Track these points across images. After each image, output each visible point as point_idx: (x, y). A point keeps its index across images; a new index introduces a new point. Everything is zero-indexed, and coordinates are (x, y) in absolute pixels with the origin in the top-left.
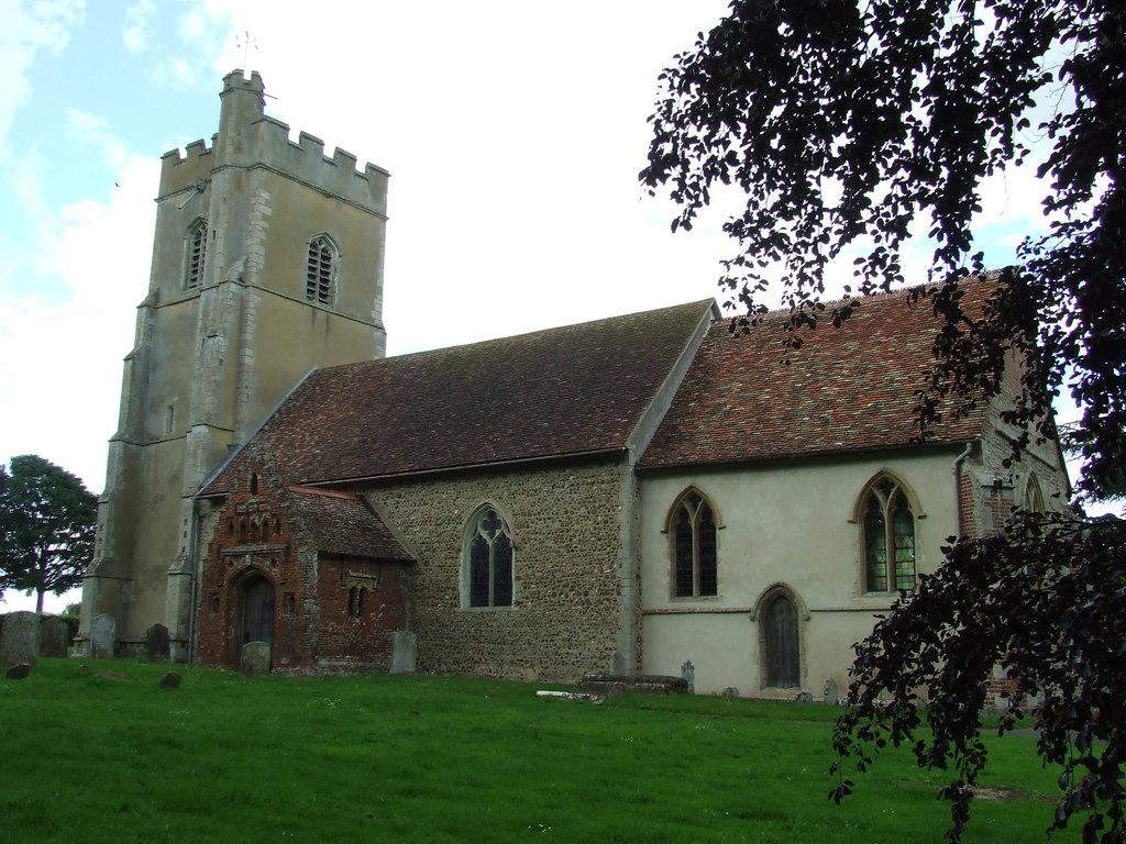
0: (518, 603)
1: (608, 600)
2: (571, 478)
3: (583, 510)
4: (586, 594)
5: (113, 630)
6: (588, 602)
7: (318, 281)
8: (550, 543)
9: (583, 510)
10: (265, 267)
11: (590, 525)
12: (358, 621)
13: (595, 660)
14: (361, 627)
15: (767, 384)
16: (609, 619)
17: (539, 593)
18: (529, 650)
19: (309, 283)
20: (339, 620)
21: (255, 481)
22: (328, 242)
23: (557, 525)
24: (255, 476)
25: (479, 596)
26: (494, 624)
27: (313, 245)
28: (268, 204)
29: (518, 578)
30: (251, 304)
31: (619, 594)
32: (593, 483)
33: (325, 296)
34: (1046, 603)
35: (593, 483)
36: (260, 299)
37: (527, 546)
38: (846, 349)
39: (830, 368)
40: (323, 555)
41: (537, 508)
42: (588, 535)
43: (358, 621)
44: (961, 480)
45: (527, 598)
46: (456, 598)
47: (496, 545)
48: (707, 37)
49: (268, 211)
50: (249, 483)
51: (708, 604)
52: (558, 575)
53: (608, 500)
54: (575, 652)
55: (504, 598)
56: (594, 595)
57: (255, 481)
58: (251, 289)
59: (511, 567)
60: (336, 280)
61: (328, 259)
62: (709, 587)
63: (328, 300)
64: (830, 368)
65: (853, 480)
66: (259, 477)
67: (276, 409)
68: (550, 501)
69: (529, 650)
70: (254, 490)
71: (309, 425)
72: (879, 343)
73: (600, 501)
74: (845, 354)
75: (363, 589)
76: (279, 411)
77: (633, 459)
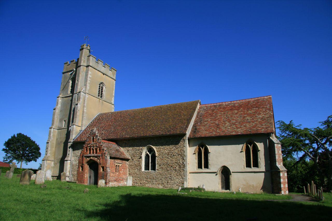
0: (157, 170)
2: (172, 140)
5: (51, 173)
7: (100, 93)
10: (89, 89)
12: (117, 173)
14: (118, 175)
15: (217, 120)
19: (99, 93)
20: (113, 173)
21: (93, 139)
22: (103, 84)
24: (93, 137)
25: (147, 168)
26: (151, 175)
27: (100, 85)
28: (90, 75)
29: (157, 164)
30: (86, 97)
32: (177, 141)
33: (102, 97)
35: (177, 141)
36: (88, 96)
38: (234, 112)
39: (232, 116)
40: (111, 158)
43: (117, 173)
45: (160, 168)
46: (141, 168)
49: (91, 76)
51: (207, 170)
55: (154, 168)
57: (93, 139)
58: (86, 94)
59: (155, 161)
60: (104, 93)
61: (103, 88)
62: (206, 166)
63: (102, 98)
64: (232, 116)
66: (94, 137)
67: (90, 122)
71: (100, 126)
72: (242, 111)
74: (235, 113)
75: (119, 166)
76: (91, 122)
77: (188, 136)
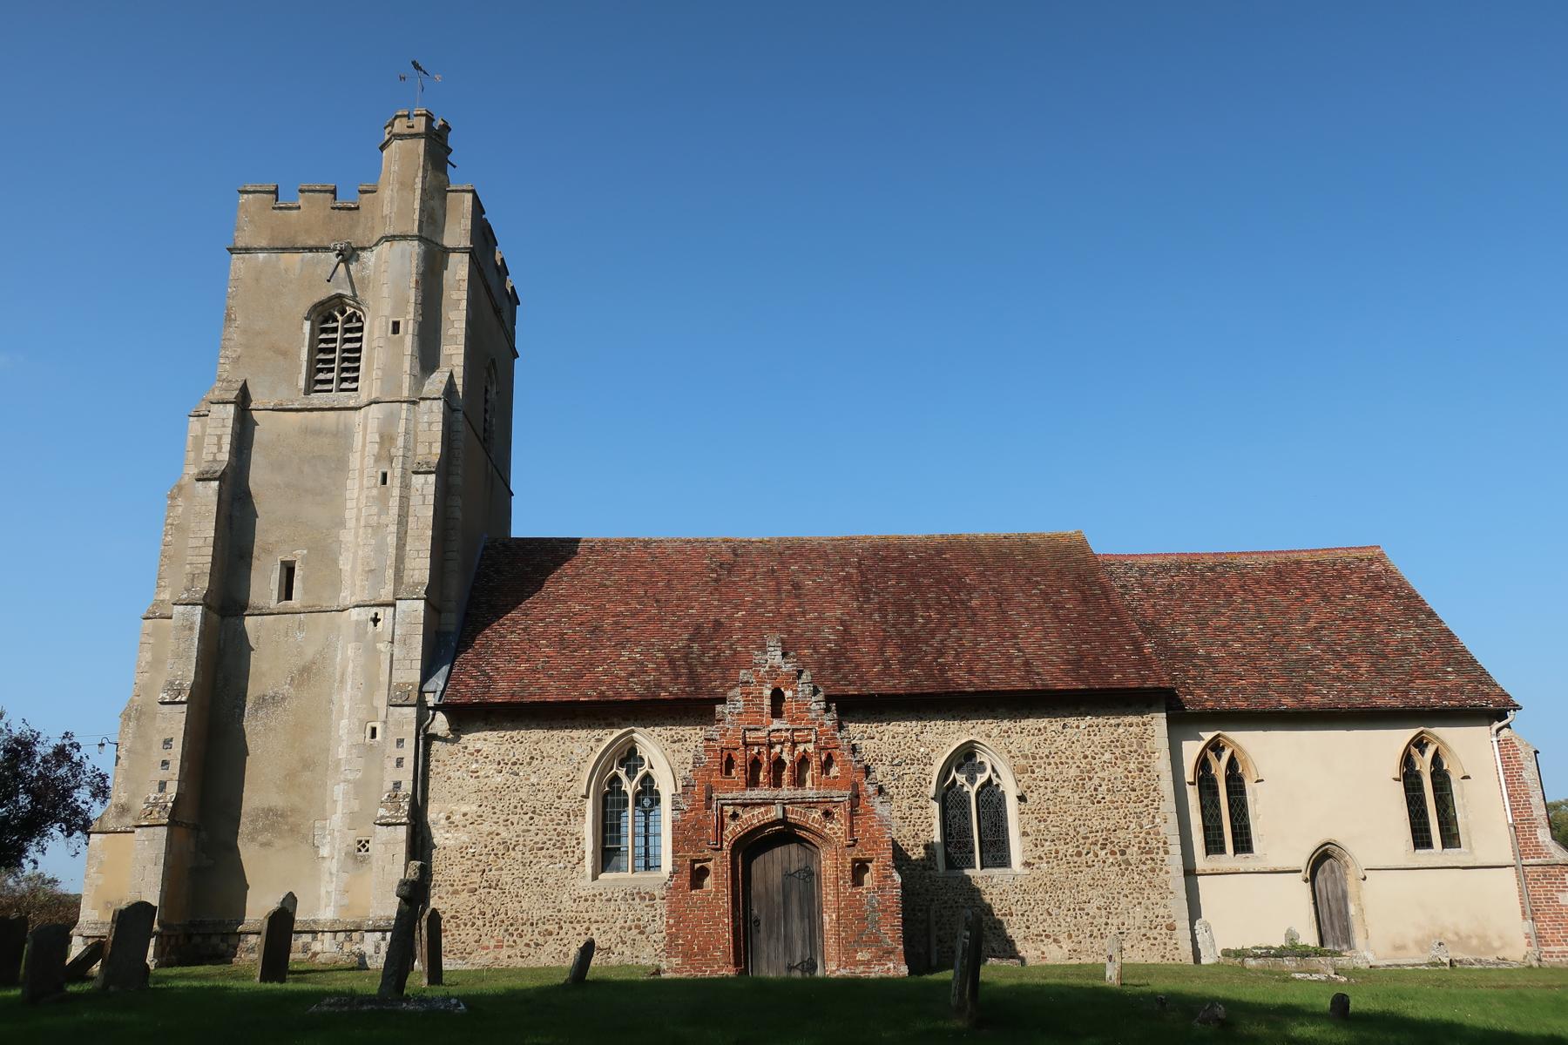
1: (1153, 859)
3: (1107, 756)
4: (1123, 853)
6: (1128, 863)
8: (1068, 793)
9: (1107, 756)
11: (1119, 772)
13: (1143, 931)
16: (1157, 882)
17: (1057, 852)
18: (1049, 921)
23: (1073, 772)
31: (1166, 852)
32: (1119, 725)
34: (1416, 619)
35: (1119, 725)
37: (1035, 795)
41: (1044, 751)
42: (1118, 783)
44: (1505, 745)
45: (1040, 858)
47: (978, 794)
48: (1497, 725)
50: (767, 702)
52: (1082, 831)
53: (1140, 746)
54: (1115, 922)
56: (1133, 853)
65: (1398, 738)
68: (1061, 742)
69: (1049, 921)
70: (777, 713)
73: (1130, 746)
